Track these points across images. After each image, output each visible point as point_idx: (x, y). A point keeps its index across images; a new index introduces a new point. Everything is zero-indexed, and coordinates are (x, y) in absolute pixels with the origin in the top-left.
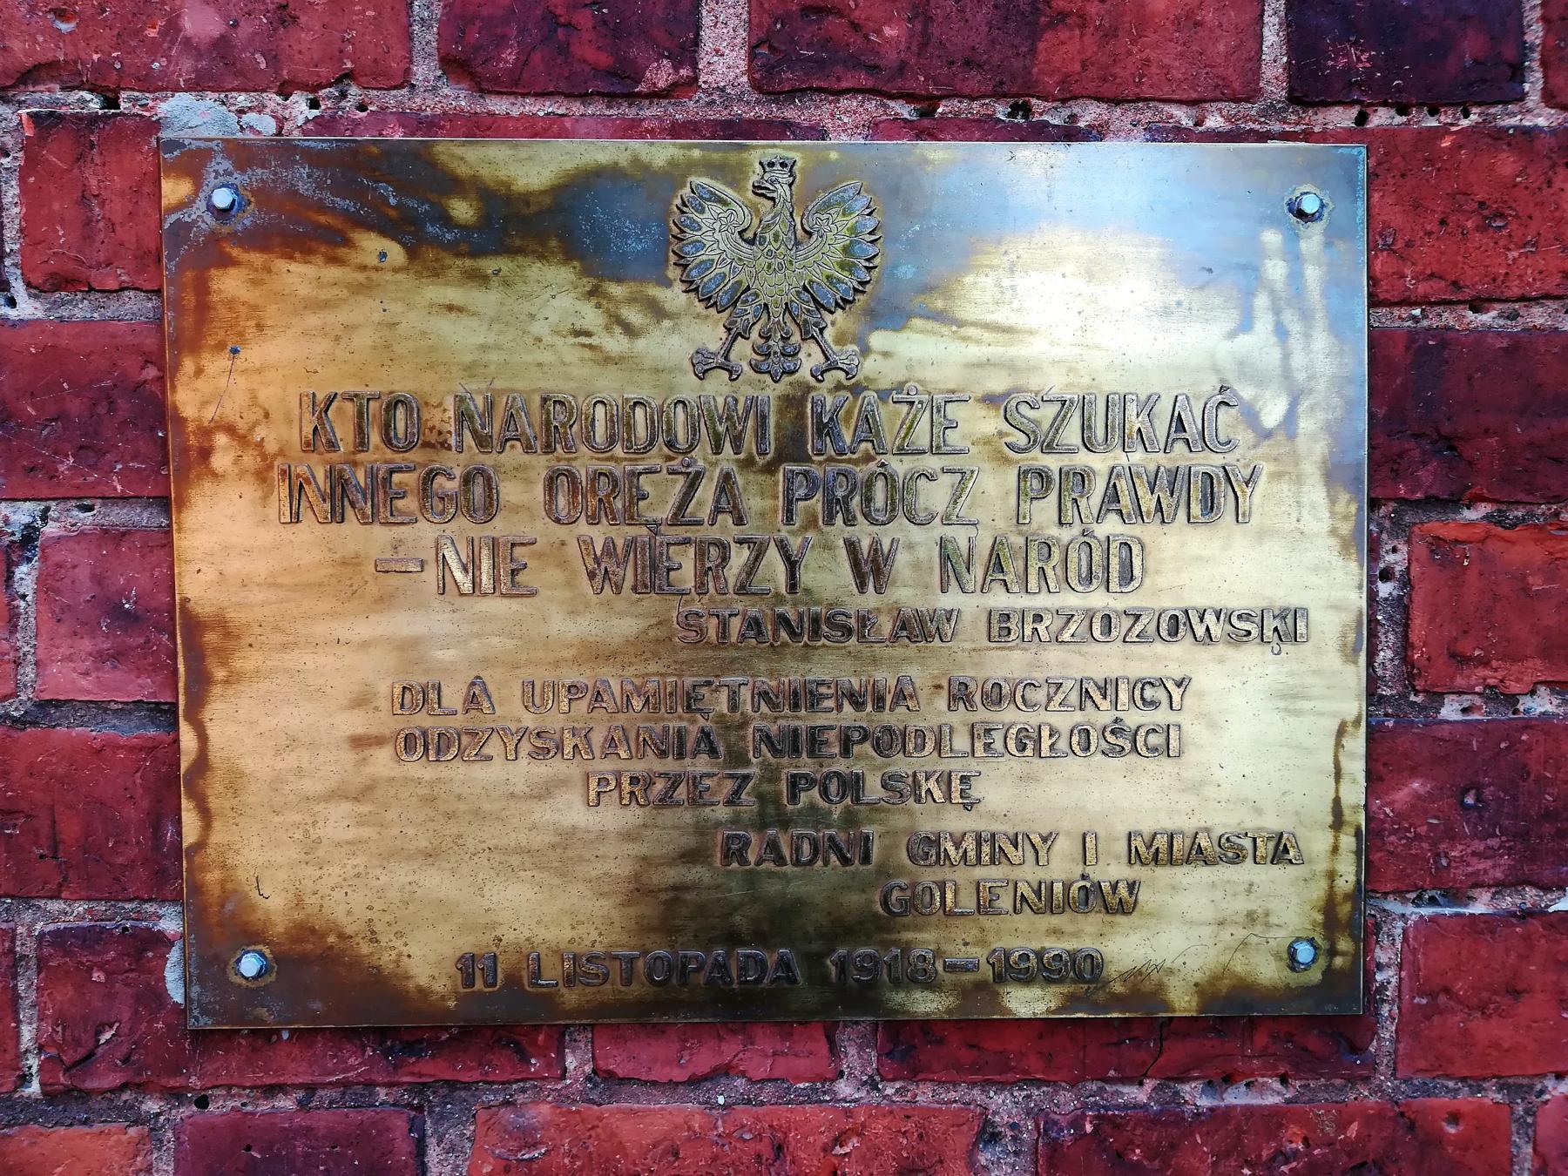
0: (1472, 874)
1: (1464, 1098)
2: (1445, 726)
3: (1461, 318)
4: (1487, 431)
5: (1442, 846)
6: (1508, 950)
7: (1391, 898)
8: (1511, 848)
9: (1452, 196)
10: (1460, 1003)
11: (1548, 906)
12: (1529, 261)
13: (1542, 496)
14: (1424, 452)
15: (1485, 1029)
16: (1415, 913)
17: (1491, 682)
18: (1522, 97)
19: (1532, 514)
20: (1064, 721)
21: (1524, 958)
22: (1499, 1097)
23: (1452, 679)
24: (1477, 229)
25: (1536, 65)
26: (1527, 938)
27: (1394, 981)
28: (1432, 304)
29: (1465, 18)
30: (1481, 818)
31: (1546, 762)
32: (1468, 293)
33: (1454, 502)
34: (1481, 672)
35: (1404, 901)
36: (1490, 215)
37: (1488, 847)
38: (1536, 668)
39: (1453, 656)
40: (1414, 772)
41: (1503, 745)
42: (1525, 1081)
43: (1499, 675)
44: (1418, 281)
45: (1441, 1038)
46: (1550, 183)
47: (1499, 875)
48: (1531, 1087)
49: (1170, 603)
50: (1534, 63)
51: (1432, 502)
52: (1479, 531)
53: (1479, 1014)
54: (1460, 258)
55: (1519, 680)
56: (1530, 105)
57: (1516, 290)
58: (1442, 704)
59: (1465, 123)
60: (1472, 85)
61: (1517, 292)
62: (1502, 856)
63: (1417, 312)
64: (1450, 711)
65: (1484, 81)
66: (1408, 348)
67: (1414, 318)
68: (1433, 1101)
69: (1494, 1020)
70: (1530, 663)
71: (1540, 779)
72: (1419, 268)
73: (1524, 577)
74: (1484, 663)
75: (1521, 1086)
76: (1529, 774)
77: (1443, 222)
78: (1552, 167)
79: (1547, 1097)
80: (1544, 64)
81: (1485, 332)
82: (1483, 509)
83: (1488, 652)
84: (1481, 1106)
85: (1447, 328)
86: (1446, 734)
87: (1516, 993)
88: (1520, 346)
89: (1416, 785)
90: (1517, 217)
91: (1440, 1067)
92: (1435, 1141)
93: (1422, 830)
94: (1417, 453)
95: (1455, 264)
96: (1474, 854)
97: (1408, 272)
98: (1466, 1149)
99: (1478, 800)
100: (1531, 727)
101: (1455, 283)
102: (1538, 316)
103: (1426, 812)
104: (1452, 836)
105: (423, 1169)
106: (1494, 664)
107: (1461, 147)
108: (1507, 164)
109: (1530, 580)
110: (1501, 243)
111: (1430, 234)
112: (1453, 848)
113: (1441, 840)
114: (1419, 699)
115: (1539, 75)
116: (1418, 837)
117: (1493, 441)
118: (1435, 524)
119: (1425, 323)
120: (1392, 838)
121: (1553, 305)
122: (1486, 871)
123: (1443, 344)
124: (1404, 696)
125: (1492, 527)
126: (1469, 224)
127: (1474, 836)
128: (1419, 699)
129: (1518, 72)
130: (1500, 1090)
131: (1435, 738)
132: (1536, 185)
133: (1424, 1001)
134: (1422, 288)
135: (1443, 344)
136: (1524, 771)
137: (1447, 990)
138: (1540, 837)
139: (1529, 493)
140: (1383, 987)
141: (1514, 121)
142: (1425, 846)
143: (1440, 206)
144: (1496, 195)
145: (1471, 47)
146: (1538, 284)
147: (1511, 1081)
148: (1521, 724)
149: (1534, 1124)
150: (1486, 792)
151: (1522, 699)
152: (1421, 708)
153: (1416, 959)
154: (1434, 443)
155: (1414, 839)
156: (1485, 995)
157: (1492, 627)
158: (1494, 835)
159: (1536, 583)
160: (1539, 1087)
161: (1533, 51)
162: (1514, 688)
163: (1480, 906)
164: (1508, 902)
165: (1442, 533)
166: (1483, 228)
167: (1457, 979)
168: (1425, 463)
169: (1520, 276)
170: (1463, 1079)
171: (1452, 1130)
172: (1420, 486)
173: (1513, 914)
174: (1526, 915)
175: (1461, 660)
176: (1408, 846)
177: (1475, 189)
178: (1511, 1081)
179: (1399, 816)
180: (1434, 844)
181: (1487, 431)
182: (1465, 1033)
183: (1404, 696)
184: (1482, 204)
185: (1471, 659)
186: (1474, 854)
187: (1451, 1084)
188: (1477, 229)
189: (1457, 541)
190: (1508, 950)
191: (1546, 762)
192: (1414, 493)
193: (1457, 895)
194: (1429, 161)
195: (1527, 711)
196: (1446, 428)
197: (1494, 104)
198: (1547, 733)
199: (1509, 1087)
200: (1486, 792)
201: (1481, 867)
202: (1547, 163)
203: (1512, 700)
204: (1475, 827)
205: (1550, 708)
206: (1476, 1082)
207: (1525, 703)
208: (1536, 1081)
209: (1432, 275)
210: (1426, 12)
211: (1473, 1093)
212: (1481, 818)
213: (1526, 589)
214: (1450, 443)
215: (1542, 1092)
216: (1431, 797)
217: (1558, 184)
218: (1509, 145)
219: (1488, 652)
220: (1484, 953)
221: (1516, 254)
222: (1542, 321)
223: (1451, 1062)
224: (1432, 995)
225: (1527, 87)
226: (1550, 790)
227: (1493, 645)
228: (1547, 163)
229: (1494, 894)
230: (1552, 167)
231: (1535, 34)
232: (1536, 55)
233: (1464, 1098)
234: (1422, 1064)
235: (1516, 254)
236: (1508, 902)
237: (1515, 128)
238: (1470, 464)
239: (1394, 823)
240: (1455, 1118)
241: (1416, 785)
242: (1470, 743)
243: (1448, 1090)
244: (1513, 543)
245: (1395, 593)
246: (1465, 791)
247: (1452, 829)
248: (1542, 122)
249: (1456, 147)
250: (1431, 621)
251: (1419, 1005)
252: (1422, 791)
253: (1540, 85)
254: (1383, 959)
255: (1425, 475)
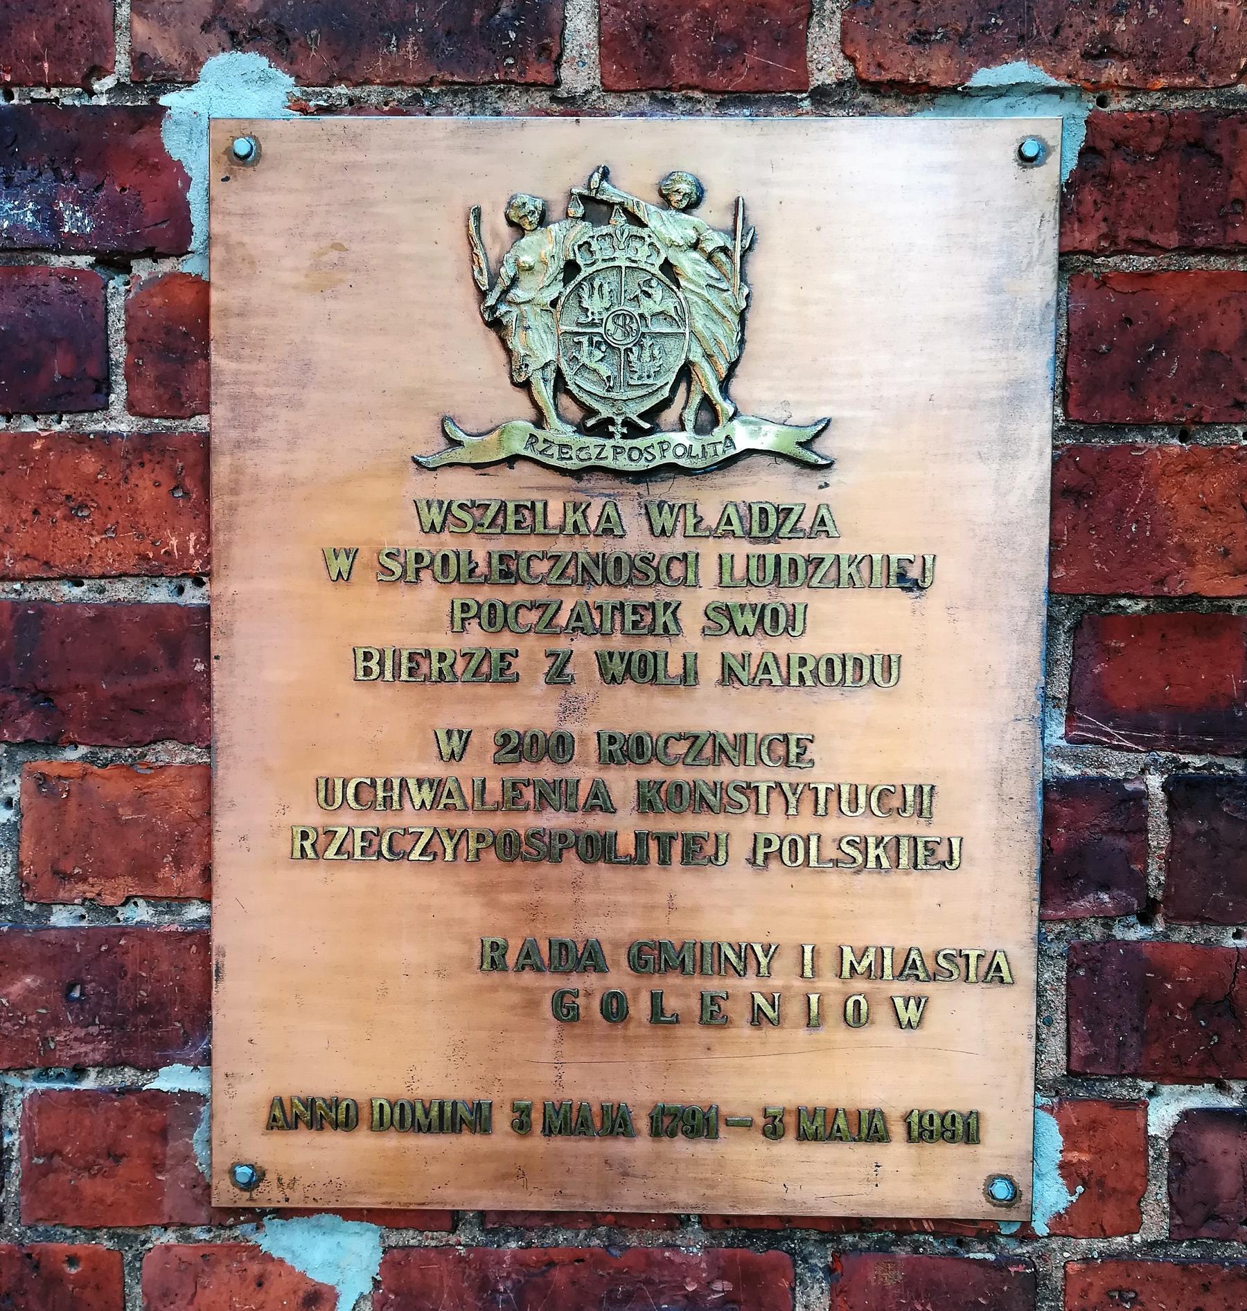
0: (75, 1056)
1: (81, 1244)
2: (53, 932)
3: (55, 591)
4: (77, 686)
5: (49, 1032)
6: (107, 1121)
7: (12, 1073)
8: (108, 1035)
9: (44, 490)
10: (70, 1164)
11: (144, 1085)
12: (109, 546)
13: (125, 741)
14: (22, 704)
15: (90, 1187)
16: (33, 1086)
17: (89, 895)
18: (106, 406)
19: (119, 756)
20: (424, 824)
21: (122, 1128)
22: (109, 1244)
23: (56, 893)
24: (64, 518)
25: (120, 379)
26: (123, 1110)
27: (17, 1143)
28: (29, 580)
29: (54, 341)
30: (82, 1009)
31: (142, 962)
32: (56, 572)
33: (54, 743)
34: (81, 887)
35: (23, 1077)
36: (75, 507)
37: (87, 1034)
38: (126, 885)
39: (56, 873)
40: (27, 969)
41: (103, 948)
42: (132, 1231)
43: (96, 890)
44: (16, 560)
45: (55, 1193)
46: (126, 480)
47: (98, 1057)
48: (136, 1237)
49: (834, 648)
50: (119, 378)
51: (29, 744)
52: (77, 770)
53: (86, 1174)
54: (51, 543)
55: (113, 894)
56: (114, 413)
57: (98, 569)
58: (51, 913)
59: (57, 428)
60: (59, 397)
61: (99, 571)
62: (101, 1041)
63: (17, 586)
64: (61, 918)
65: (71, 394)
66: (12, 616)
67: (16, 591)
68: (52, 1246)
69: (99, 1179)
70: (121, 880)
71: (136, 977)
72: (17, 550)
73: (116, 808)
74: (83, 879)
75: (128, 1236)
76: (126, 974)
77: (36, 512)
78: (129, 466)
79: (150, 1246)
80: (127, 377)
81: (71, 605)
82: (83, 750)
83: (85, 871)
84: (96, 1252)
85: (44, 601)
86: (52, 938)
87: (118, 1158)
88: (105, 616)
89: (28, 980)
90: (98, 508)
91: (57, 1216)
92: (55, 1280)
93: (32, 1018)
94: (16, 704)
95: (46, 547)
96: (76, 1039)
97: (7, 553)
98: (83, 1287)
99: (81, 994)
100: (128, 934)
101: (46, 563)
102: (121, 591)
103: (36, 1004)
104: (57, 1023)
105: (125, 1308)
106: (91, 880)
107: (49, 450)
108: (89, 463)
109: (120, 811)
110: (86, 530)
111: (24, 522)
112: (58, 1033)
113: (48, 1027)
114: (32, 908)
115: (124, 387)
116: (28, 1023)
117: (83, 695)
118: (41, 762)
119: (27, 595)
120: (8, 1024)
121: (132, 582)
122: (86, 1053)
123: (41, 614)
124: (19, 906)
125: (88, 766)
126: (58, 514)
127: (76, 1024)
128: (32, 908)
129: (103, 386)
130: (110, 1238)
131: (44, 942)
132: (114, 481)
133: (41, 1161)
134: (19, 567)
135: (41, 614)
136: (121, 971)
137: (60, 1153)
138: (136, 1026)
139: (115, 739)
140: (9, 1149)
141: (99, 427)
142: (35, 1031)
143: (33, 500)
144: (80, 490)
145: (59, 366)
146: (117, 565)
147: (119, 1231)
148: (118, 931)
149: (140, 1269)
150: (88, 987)
151: (120, 910)
152: (35, 916)
153: (31, 1125)
154: (33, 695)
155: (25, 1026)
156: (90, 1158)
157: (88, 850)
158: (94, 1024)
159: (126, 814)
160: (143, 1237)
161: (118, 367)
162: (109, 900)
163: (89, 1083)
164: (112, 1080)
165: (47, 770)
166: (69, 518)
167: (66, 1144)
168: (23, 713)
169: (101, 558)
170: (76, 1228)
171: (73, 1271)
172: (20, 732)
173: (113, 1091)
174: (125, 1091)
175: (63, 876)
176: (21, 1031)
177: (63, 485)
178: (119, 1231)
179: (14, 1006)
180: (42, 1030)
181: (77, 686)
182: (76, 1189)
183: (19, 906)
184: (68, 497)
185: (71, 876)
186: (76, 1039)
187: (69, 1232)
188: (64, 518)
189: (59, 777)
190: (107, 1121)
191: (142, 962)
192: (15, 737)
193: (79, 1072)
194: (24, 461)
195: (126, 920)
196: (42, 683)
197: (82, 412)
198: (141, 939)
199: (119, 1237)
200: (88, 987)
201: (82, 1050)
202: (124, 463)
203: (111, 911)
204: (77, 1017)
205: (146, 918)
206: (92, 1231)
207: (123, 913)
208: (140, 1231)
209: (27, 556)
210: (21, 335)
211: (89, 1241)
212: (82, 1009)
213: (117, 818)
214: (47, 696)
215: (144, 1243)
216: (40, 991)
217: (133, 481)
218: (90, 447)
219: (85, 871)
220: (87, 1122)
221: (98, 539)
222: (125, 595)
223: (64, 1212)
224: (50, 1156)
225: (113, 397)
226: (144, 987)
227: (90, 864)
228: (124, 463)
229: (99, 1072)
230: (129, 466)
231: (119, 353)
232: (121, 371)
233: (81, 1244)
234: (41, 1214)
235: (98, 539)
236: (112, 1080)
237: (96, 433)
238: (63, 713)
239: (9, 1011)
240: (72, 1260)
241: (28, 980)
242: (74, 946)
243: (67, 1237)
244: (108, 779)
245: (13, 819)
246: (71, 987)
247: (58, 1018)
248: (124, 428)
249: (46, 450)
250: (37, 843)
251: (37, 1165)
252: (33, 985)
253: (124, 396)
254: (12, 1124)
255: (24, 723)
